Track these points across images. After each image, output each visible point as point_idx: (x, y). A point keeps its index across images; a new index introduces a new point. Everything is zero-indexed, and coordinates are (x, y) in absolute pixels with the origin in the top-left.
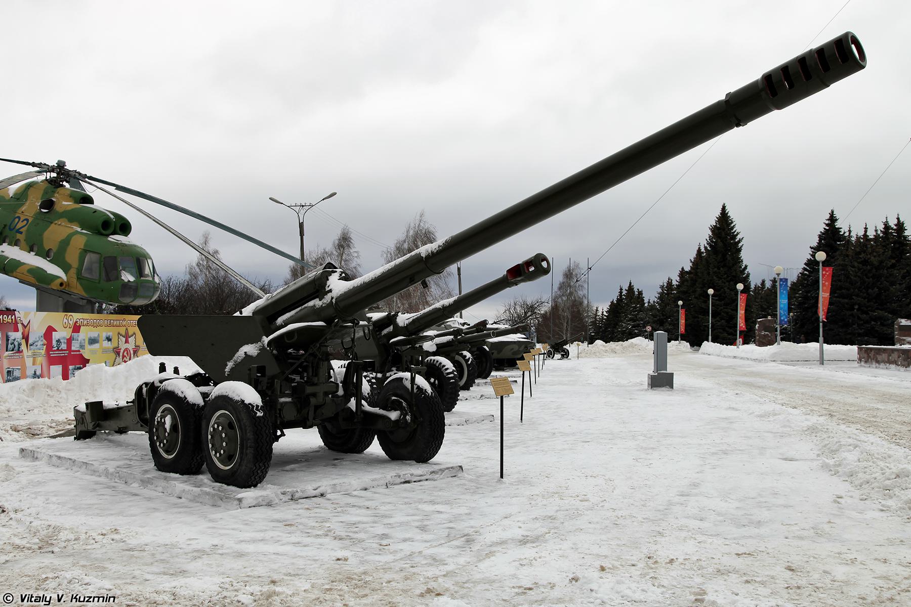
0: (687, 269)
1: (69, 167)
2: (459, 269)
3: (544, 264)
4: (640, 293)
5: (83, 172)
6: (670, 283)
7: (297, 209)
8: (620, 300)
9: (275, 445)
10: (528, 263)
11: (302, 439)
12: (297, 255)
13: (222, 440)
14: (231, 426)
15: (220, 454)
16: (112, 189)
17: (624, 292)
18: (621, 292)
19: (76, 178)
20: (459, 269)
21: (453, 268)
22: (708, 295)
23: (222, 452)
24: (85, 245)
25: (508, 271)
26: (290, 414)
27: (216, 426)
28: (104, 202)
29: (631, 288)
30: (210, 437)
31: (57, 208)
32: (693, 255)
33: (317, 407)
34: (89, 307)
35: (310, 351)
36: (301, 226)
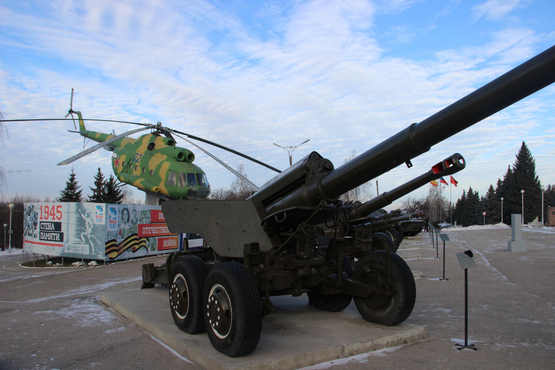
0: (502, 180)
1: (163, 125)
2: (377, 182)
3: (461, 161)
4: (477, 194)
5: (170, 128)
6: (491, 188)
7: (288, 149)
8: (463, 197)
10: (449, 160)
16: (186, 137)
17: (466, 194)
18: (464, 194)
19: (167, 132)
20: (377, 182)
21: (373, 181)
22: (521, 194)
23: (217, 323)
24: (169, 167)
25: (433, 168)
27: (213, 299)
28: (181, 143)
29: (471, 190)
31: (157, 147)
32: (505, 172)
35: (298, 229)
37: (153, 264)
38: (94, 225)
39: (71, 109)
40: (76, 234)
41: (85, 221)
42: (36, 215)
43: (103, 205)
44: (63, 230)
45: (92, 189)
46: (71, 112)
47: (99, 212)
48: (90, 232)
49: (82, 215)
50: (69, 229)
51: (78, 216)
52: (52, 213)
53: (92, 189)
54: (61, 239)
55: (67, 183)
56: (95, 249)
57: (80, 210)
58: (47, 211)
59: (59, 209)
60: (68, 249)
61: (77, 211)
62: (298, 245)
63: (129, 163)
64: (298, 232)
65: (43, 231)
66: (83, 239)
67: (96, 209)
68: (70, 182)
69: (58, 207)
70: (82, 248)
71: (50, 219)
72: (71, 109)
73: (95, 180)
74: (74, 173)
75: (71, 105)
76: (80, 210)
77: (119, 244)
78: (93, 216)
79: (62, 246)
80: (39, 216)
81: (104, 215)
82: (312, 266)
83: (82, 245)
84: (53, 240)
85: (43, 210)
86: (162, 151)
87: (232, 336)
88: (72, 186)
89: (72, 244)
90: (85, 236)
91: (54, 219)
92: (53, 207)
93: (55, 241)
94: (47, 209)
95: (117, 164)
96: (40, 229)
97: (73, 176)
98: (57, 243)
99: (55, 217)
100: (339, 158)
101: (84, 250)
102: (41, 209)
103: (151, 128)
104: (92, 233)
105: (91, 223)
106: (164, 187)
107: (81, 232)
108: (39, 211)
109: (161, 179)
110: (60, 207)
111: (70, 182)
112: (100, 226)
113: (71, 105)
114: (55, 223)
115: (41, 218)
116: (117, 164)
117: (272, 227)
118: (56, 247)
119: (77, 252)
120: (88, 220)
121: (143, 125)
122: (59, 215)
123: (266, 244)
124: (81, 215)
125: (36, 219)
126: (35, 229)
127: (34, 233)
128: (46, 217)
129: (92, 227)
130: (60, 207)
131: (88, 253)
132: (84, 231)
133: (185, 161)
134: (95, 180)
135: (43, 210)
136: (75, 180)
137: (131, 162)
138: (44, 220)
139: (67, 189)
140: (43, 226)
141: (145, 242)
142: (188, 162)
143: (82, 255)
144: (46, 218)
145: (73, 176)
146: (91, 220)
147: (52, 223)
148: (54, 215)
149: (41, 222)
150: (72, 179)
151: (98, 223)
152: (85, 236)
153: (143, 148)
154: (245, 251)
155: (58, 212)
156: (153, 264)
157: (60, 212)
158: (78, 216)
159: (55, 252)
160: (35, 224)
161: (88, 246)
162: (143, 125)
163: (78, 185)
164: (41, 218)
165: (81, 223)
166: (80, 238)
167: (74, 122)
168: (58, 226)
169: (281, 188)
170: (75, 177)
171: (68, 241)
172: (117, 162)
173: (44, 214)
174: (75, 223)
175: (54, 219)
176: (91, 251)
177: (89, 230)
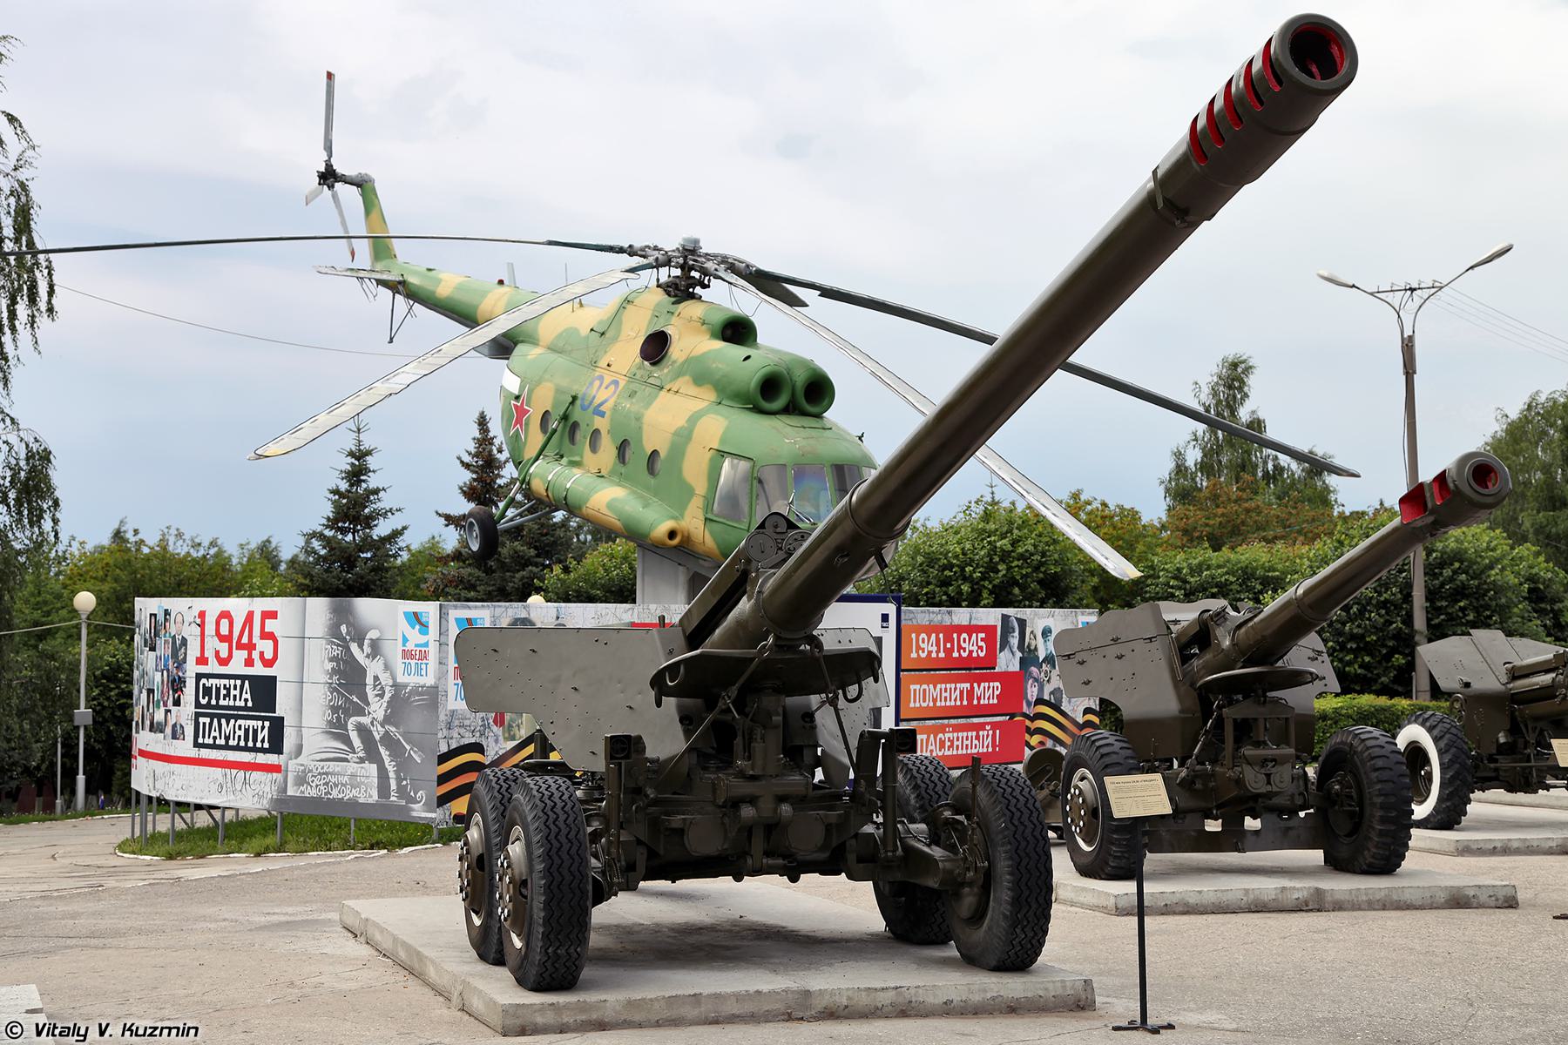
7: (1395, 299)
36: (1408, 347)
38: (395, 685)
39: (329, 166)
40: (330, 723)
41: (363, 671)
42: (179, 646)
43: (430, 609)
44: (283, 707)
45: (450, 519)
46: (329, 177)
47: (415, 636)
48: (380, 715)
49: (354, 647)
50: (305, 702)
51: (337, 652)
52: (245, 640)
53: (450, 519)
54: (276, 746)
55: (336, 492)
56: (399, 780)
57: (344, 629)
58: (224, 630)
59: (270, 625)
60: (301, 780)
61: (334, 632)
63: (565, 417)
65: (210, 709)
66: (357, 742)
67: (403, 625)
68: (344, 486)
70: (353, 776)
71: (237, 666)
72: (329, 166)
73: (467, 476)
74: (365, 446)
75: (329, 148)
76: (344, 629)
77: (496, 763)
78: (393, 650)
79: (275, 769)
80: (193, 652)
81: (433, 650)
82: (782, 799)
83: (352, 767)
84: (246, 749)
85: (210, 629)
86: (701, 375)
88: (353, 507)
89: (318, 762)
90: (363, 731)
91: (249, 662)
92: (250, 617)
93: (255, 750)
94: (225, 623)
95: (519, 421)
96: (198, 705)
97: (360, 455)
98: (261, 758)
99: (255, 655)
100: (1271, 434)
101: (360, 784)
102: (202, 626)
103: (658, 265)
104: (387, 720)
105: (385, 679)
106: (701, 524)
107: (348, 715)
108: (191, 634)
109: (689, 492)
110: (272, 615)
111: (344, 486)
112: (417, 690)
113: (329, 148)
115: (202, 660)
116: (519, 421)
118: (256, 775)
119: (335, 794)
120: (373, 668)
121: (621, 250)
122: (266, 647)
124: (348, 649)
125: (181, 664)
126: (177, 703)
127: (172, 721)
128: (224, 654)
129: (387, 696)
130: (272, 615)
131: (374, 797)
132: (361, 712)
133: (791, 409)
134: (467, 476)
135: (210, 629)
136: (373, 481)
137: (577, 415)
138: (213, 667)
139: (332, 523)
140: (207, 691)
143: (353, 803)
144: (224, 662)
145: (360, 455)
146: (387, 667)
147: (243, 678)
148: (251, 647)
149: (199, 677)
150: (356, 474)
151: (412, 680)
152: (363, 731)
153: (626, 353)
155: (266, 635)
157: (270, 636)
158: (337, 652)
159: (250, 796)
160: (177, 685)
161: (373, 769)
162: (621, 250)
163: (385, 501)
165: (349, 677)
166: (347, 740)
167: (346, 230)
168: (264, 690)
170: (371, 462)
171: (299, 750)
172: (521, 412)
173: (213, 644)
174: (326, 678)
176: (383, 789)
177: (378, 708)
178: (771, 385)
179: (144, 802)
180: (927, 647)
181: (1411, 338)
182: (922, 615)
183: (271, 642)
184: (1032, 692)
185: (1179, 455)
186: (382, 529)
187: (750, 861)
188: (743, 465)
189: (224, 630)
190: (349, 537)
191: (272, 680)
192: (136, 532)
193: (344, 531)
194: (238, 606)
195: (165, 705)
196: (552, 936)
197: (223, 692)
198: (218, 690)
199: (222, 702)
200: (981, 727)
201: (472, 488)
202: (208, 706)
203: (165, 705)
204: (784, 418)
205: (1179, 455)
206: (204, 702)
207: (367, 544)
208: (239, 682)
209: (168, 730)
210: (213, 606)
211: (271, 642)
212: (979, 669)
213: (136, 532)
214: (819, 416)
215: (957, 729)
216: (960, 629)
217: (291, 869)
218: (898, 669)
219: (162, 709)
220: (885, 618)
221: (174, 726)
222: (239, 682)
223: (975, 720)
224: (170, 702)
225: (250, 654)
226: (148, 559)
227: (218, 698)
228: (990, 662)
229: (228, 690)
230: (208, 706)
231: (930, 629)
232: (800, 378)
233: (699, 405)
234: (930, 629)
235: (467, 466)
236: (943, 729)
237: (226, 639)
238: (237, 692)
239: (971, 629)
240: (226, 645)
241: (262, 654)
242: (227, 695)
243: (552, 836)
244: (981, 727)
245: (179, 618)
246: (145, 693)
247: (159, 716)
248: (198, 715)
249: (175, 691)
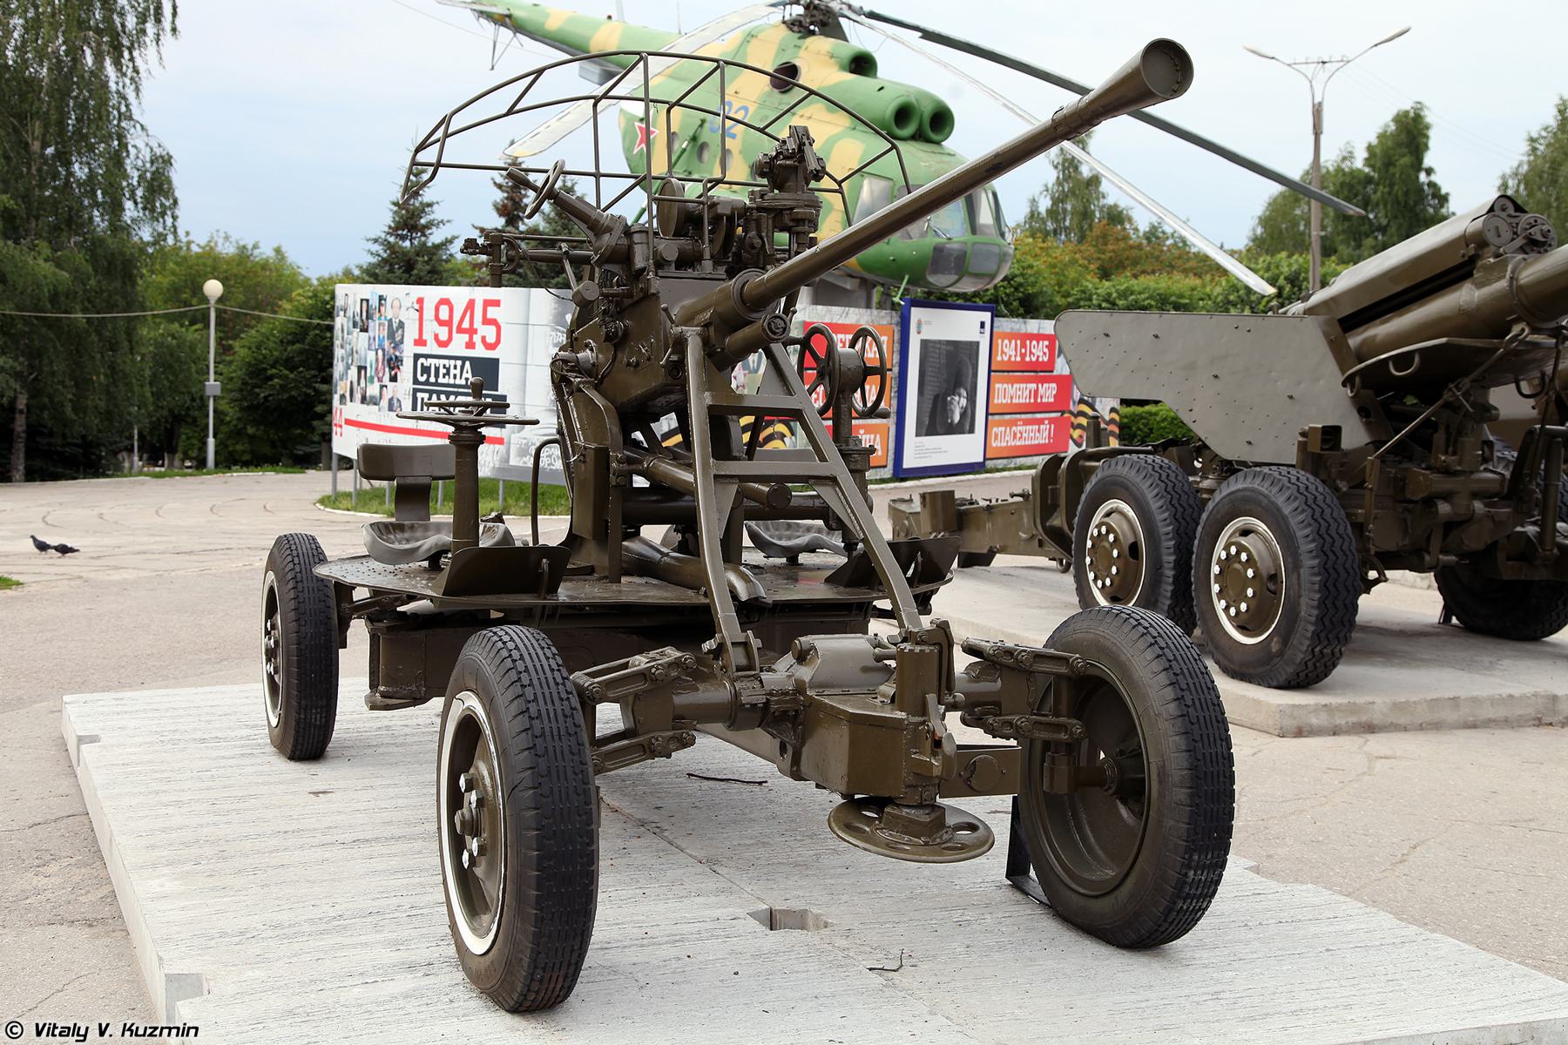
9: (1363, 600)
11: (1406, 597)
12: (633, 181)
13: (1246, 582)
14: (1134, 549)
15: (1238, 612)
26: (1384, 536)
30: (1216, 569)
33: (1450, 526)
34: (862, 294)
35: (1447, 396)
36: (1317, 112)
37: (952, 493)
42: (395, 332)
52: (466, 325)
58: (444, 315)
59: (492, 312)
62: (1439, 438)
63: (694, 139)
64: (1447, 405)
69: (489, 303)
71: (458, 346)
73: (499, 196)
80: (411, 333)
85: (429, 313)
87: (1286, 633)
91: (471, 345)
92: (471, 305)
96: (416, 381)
99: (477, 339)
102: (420, 311)
110: (497, 303)
114: (475, 362)
115: (420, 342)
117: (1375, 390)
122: (490, 333)
123: (1354, 436)
125: (397, 345)
126: (394, 379)
127: (387, 394)
128: (444, 336)
130: (497, 303)
133: (919, 136)
134: (499, 196)
136: (427, 195)
139: (394, 230)
140: (426, 370)
141: (782, 436)
142: (929, 141)
147: (464, 359)
148: (472, 331)
149: (417, 357)
154: (1302, 447)
155: (487, 321)
156: (952, 493)
157: (494, 322)
160: (394, 363)
163: (437, 214)
164: (420, 342)
169: (1399, 288)
173: (431, 327)
175: (471, 345)
178: (903, 114)
179: (335, 460)
180: (1009, 352)
181: (1320, 104)
182: (1007, 325)
183: (493, 328)
184: (1077, 395)
185: (1034, 202)
186: (436, 237)
187: (1427, 558)
188: (883, 183)
189: (444, 315)
190: (407, 244)
191: (495, 363)
192: (188, 234)
193: (403, 238)
194: (460, 295)
195: (380, 380)
196: (1323, 635)
197: (442, 371)
198: (437, 369)
199: (441, 380)
200: (1041, 422)
201: (504, 206)
202: (427, 383)
203: (380, 380)
204: (913, 143)
205: (1034, 202)
206: (422, 379)
207: (423, 250)
208: (459, 363)
209: (384, 403)
210: (432, 293)
211: (493, 328)
212: (1039, 372)
213: (188, 234)
214: (938, 143)
215: (1027, 422)
216: (1032, 337)
217: (789, 538)
218: (990, 371)
219: (377, 385)
220: (983, 325)
221: (391, 400)
222: (459, 363)
223: (1038, 416)
224: (387, 377)
225: (471, 338)
226: (198, 256)
227: (437, 376)
228: (1049, 367)
229: (448, 370)
230: (427, 383)
231: (1012, 336)
232: (927, 110)
233: (837, 130)
234: (1012, 336)
235: (500, 186)
236: (1014, 423)
237: (448, 323)
238: (458, 372)
239: (1039, 337)
240: (446, 329)
241: (483, 339)
242: (448, 373)
243: (1323, 531)
244: (1041, 422)
245: (396, 303)
246: (353, 372)
247: (373, 390)
248: (415, 391)
249: (391, 369)
